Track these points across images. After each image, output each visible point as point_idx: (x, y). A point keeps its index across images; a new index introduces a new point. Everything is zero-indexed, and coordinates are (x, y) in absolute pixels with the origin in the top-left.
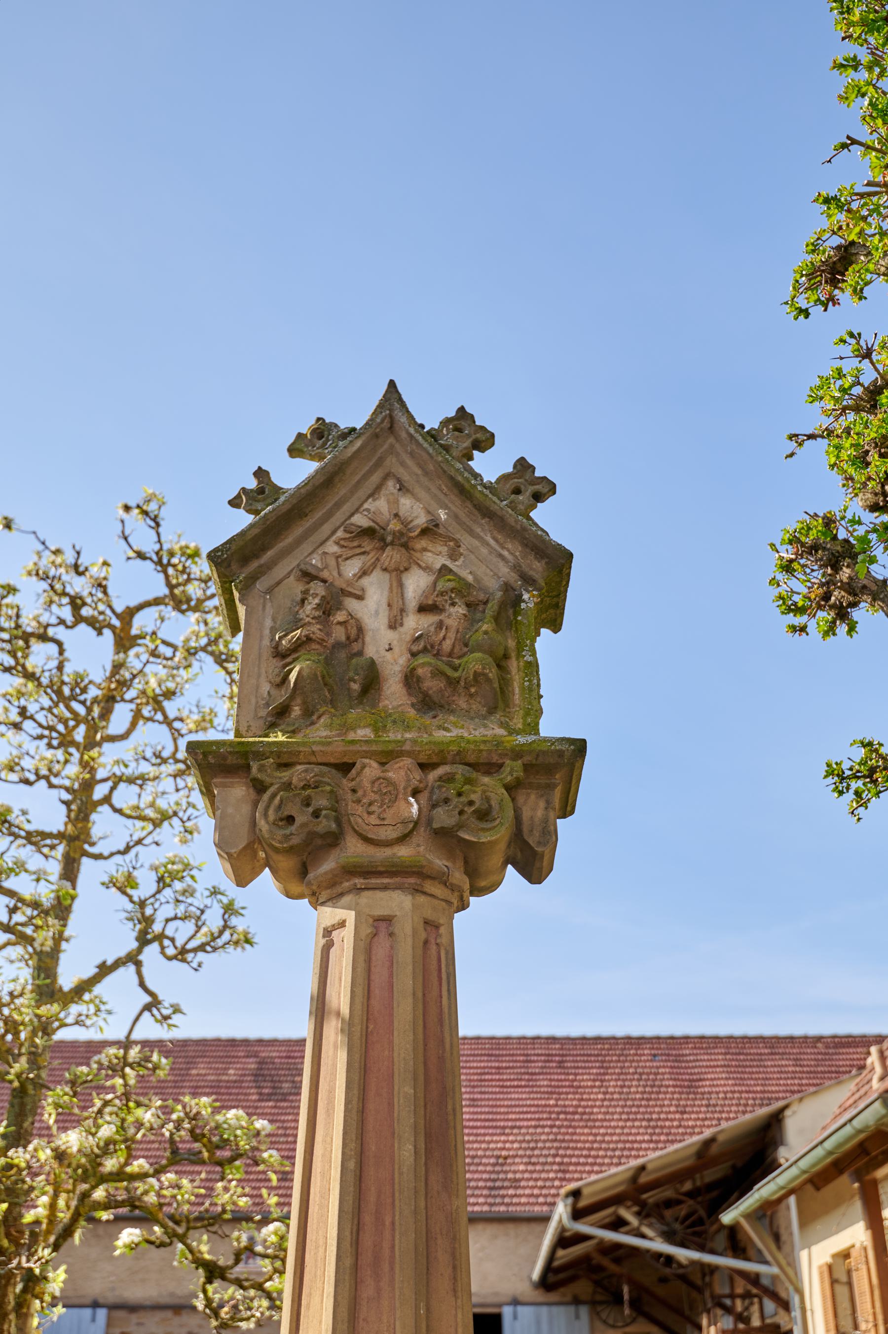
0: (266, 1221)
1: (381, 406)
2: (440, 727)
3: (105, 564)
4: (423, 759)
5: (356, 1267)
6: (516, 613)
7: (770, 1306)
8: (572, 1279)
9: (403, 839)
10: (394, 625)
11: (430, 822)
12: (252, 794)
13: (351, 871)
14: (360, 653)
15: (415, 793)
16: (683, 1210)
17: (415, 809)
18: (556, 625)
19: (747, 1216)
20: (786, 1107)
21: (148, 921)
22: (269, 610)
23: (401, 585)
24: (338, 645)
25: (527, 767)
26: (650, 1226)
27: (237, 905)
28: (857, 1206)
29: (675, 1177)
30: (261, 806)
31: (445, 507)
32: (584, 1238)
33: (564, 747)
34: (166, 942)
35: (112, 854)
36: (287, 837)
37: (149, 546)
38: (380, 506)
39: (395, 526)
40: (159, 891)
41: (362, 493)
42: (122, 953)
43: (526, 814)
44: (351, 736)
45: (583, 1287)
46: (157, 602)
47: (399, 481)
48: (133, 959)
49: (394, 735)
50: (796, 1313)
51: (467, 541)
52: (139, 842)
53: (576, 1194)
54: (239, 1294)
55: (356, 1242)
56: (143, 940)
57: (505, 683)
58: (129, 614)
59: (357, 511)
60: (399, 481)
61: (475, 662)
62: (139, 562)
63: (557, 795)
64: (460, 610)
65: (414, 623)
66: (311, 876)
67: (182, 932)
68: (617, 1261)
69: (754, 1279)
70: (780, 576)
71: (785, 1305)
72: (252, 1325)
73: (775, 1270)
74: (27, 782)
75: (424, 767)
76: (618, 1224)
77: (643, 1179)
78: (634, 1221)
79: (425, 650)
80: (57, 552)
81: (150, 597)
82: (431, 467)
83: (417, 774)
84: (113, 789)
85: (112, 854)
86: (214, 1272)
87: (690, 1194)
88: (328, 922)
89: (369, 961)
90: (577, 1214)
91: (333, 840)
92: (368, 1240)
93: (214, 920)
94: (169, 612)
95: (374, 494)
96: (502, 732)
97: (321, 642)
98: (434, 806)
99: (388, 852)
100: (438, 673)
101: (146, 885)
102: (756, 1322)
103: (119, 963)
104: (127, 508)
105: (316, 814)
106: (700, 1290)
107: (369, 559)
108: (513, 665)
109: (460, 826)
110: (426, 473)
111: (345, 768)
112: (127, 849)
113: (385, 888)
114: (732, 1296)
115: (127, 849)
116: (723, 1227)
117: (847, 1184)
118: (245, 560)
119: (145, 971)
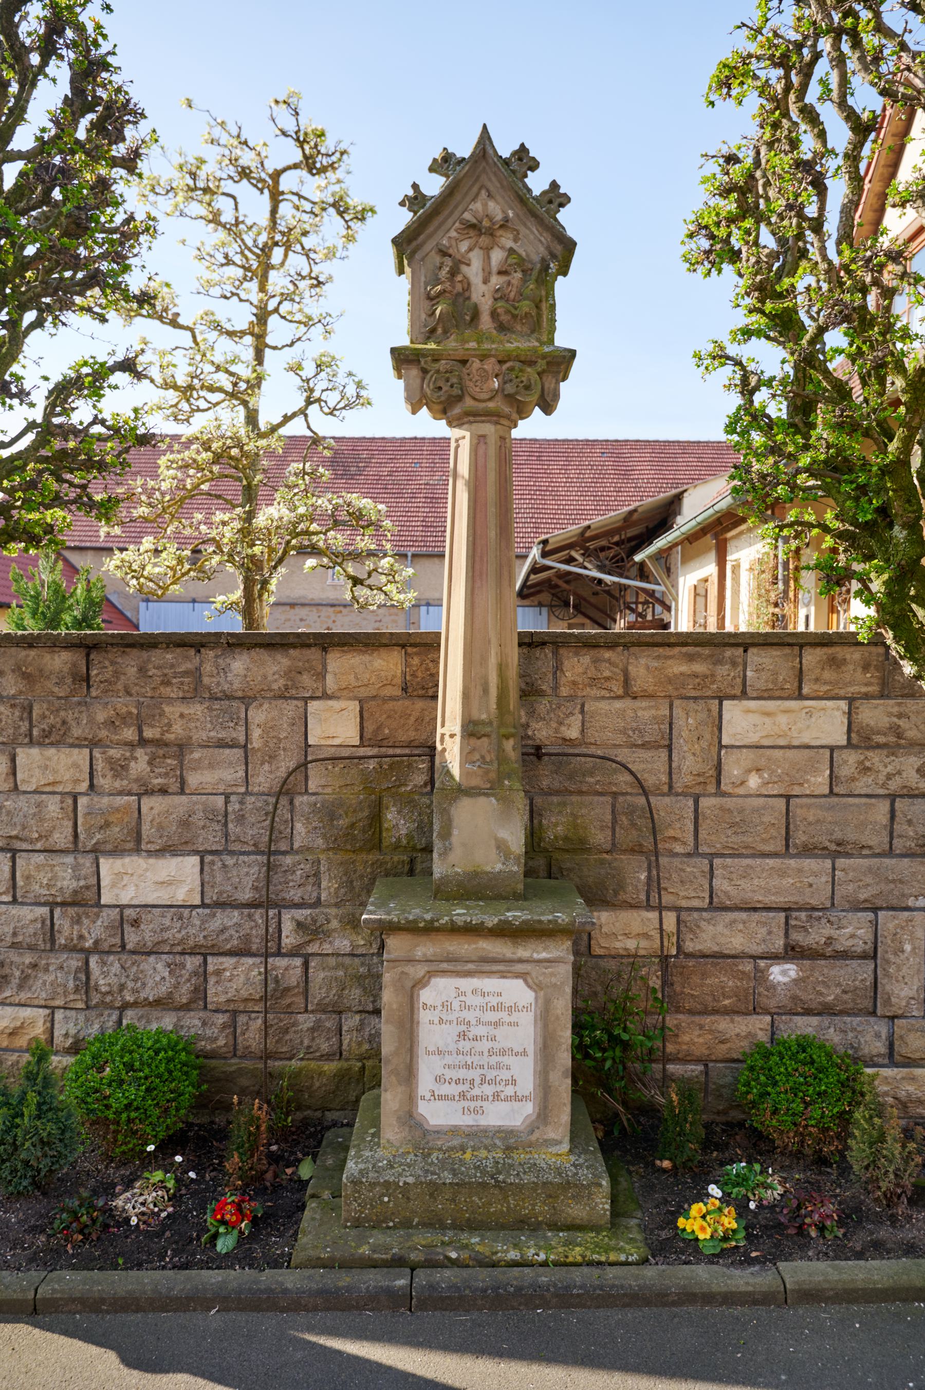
0: (385, 556)
1: (479, 143)
2: (509, 342)
3: (265, 144)
4: (500, 358)
5: (473, 576)
6: (547, 275)
7: (658, 608)
8: (539, 592)
9: (490, 399)
10: (486, 281)
11: (503, 390)
12: (421, 374)
13: (468, 414)
14: (469, 298)
15: (497, 376)
16: (611, 553)
17: (496, 385)
18: (565, 274)
19: (650, 557)
20: (685, 491)
21: (312, 390)
22: (423, 271)
23: (489, 258)
24: (458, 294)
25: (548, 363)
26: (590, 562)
27: (364, 383)
28: (712, 555)
29: (608, 533)
30: (426, 382)
31: (512, 209)
32: (550, 568)
33: (566, 354)
34: (323, 404)
35: (283, 347)
36: (439, 397)
37: (291, 128)
38: (477, 206)
39: (486, 223)
40: (317, 374)
41: (468, 199)
42: (296, 409)
43: (546, 386)
44: (467, 346)
45: (545, 597)
46: (296, 166)
47: (488, 191)
48: (303, 412)
49: (486, 346)
50: (673, 613)
51: (523, 231)
52: (299, 339)
53: (545, 542)
54: (369, 592)
55: (473, 567)
56: (309, 402)
57: (539, 315)
58: (277, 175)
59: (466, 210)
60: (488, 191)
61: (526, 306)
62: (283, 137)
63: (561, 375)
64: (519, 275)
65: (496, 281)
66: (449, 414)
67: (332, 398)
68: (567, 582)
69: (651, 594)
70: (686, 240)
71: (668, 609)
72: (375, 607)
73: (663, 588)
74: (226, 297)
75: (500, 362)
76: (570, 560)
77: (588, 534)
78: (580, 559)
79: (501, 298)
80: (222, 124)
81: (290, 162)
82: (505, 183)
83: (497, 367)
84: (280, 303)
85: (283, 347)
86: (356, 581)
87: (617, 544)
88: (458, 436)
89: (476, 455)
90: (544, 555)
91: (460, 398)
92: (477, 567)
93: (351, 391)
94: (303, 173)
95: (474, 200)
96: (537, 344)
97: (450, 292)
98: (505, 383)
99: (483, 405)
100: (508, 312)
101: (309, 370)
102: (649, 618)
103: (294, 415)
104: (277, 102)
105: (452, 386)
106: (617, 600)
107: (473, 241)
108: (544, 306)
109: (517, 393)
110: (502, 186)
111: (464, 362)
112: (292, 344)
113: (483, 422)
114: (637, 603)
115: (292, 344)
116: (636, 563)
117: (709, 540)
118: (409, 241)
119: (309, 419)
